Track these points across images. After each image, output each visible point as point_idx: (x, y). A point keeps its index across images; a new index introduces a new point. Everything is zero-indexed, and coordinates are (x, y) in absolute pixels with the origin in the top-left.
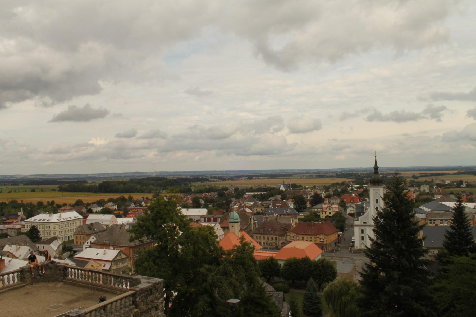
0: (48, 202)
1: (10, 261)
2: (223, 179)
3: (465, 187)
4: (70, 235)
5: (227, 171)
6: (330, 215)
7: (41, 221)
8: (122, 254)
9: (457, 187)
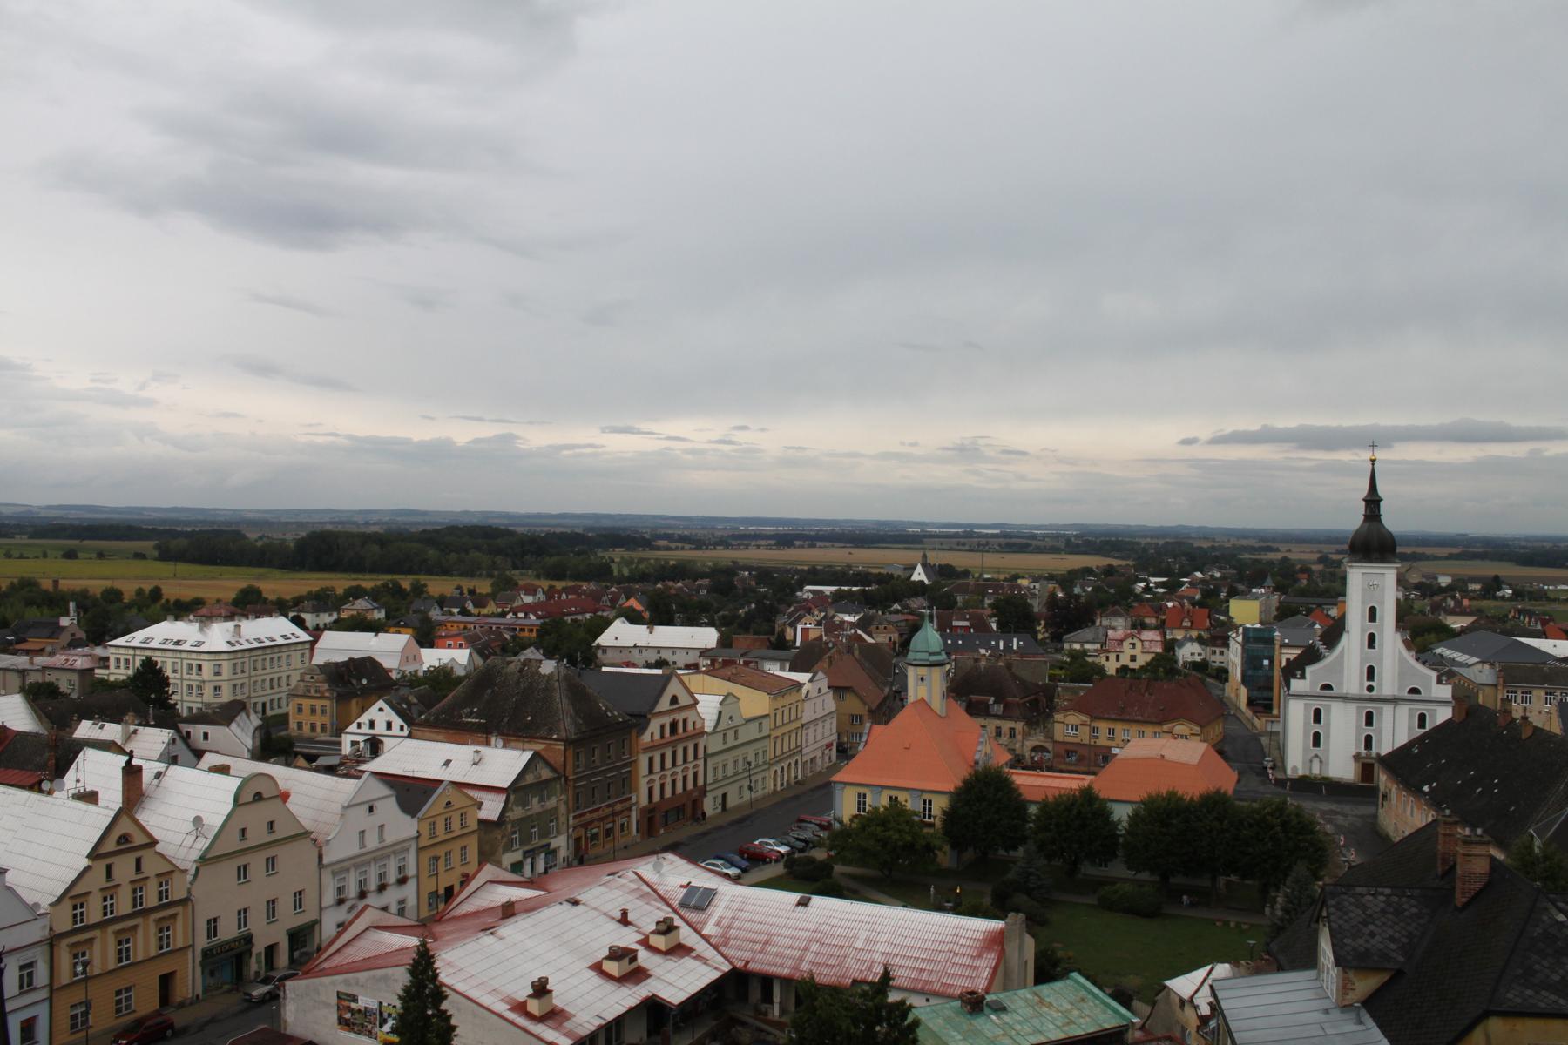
0: (140, 592)
1: (159, 775)
2: (699, 544)
3: (1510, 599)
4: (267, 699)
5: (704, 519)
6: (1132, 665)
7: (171, 646)
8: (541, 765)
9: (1484, 598)
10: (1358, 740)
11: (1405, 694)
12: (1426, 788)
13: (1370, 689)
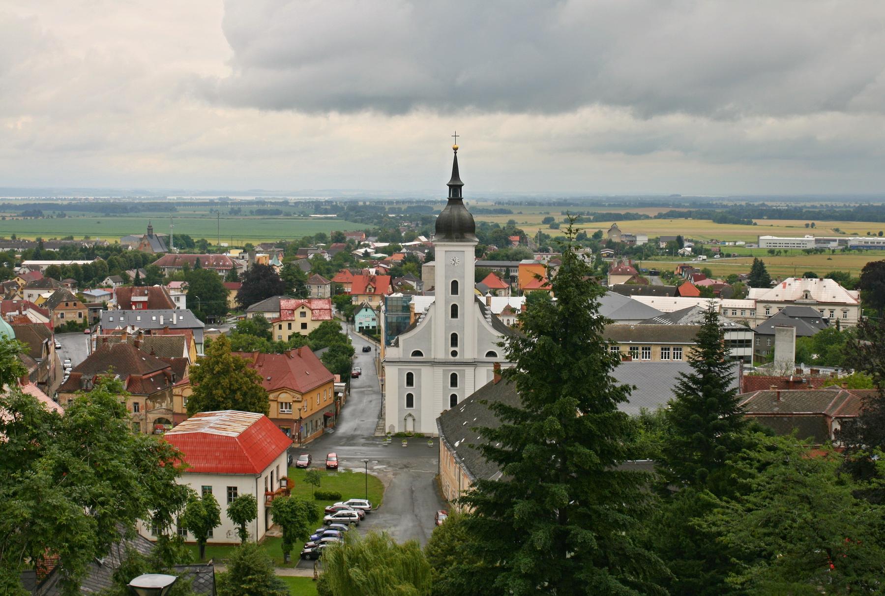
6: (304, 332)
10: (444, 400)
11: (484, 358)
12: (457, 444)
13: (454, 354)
